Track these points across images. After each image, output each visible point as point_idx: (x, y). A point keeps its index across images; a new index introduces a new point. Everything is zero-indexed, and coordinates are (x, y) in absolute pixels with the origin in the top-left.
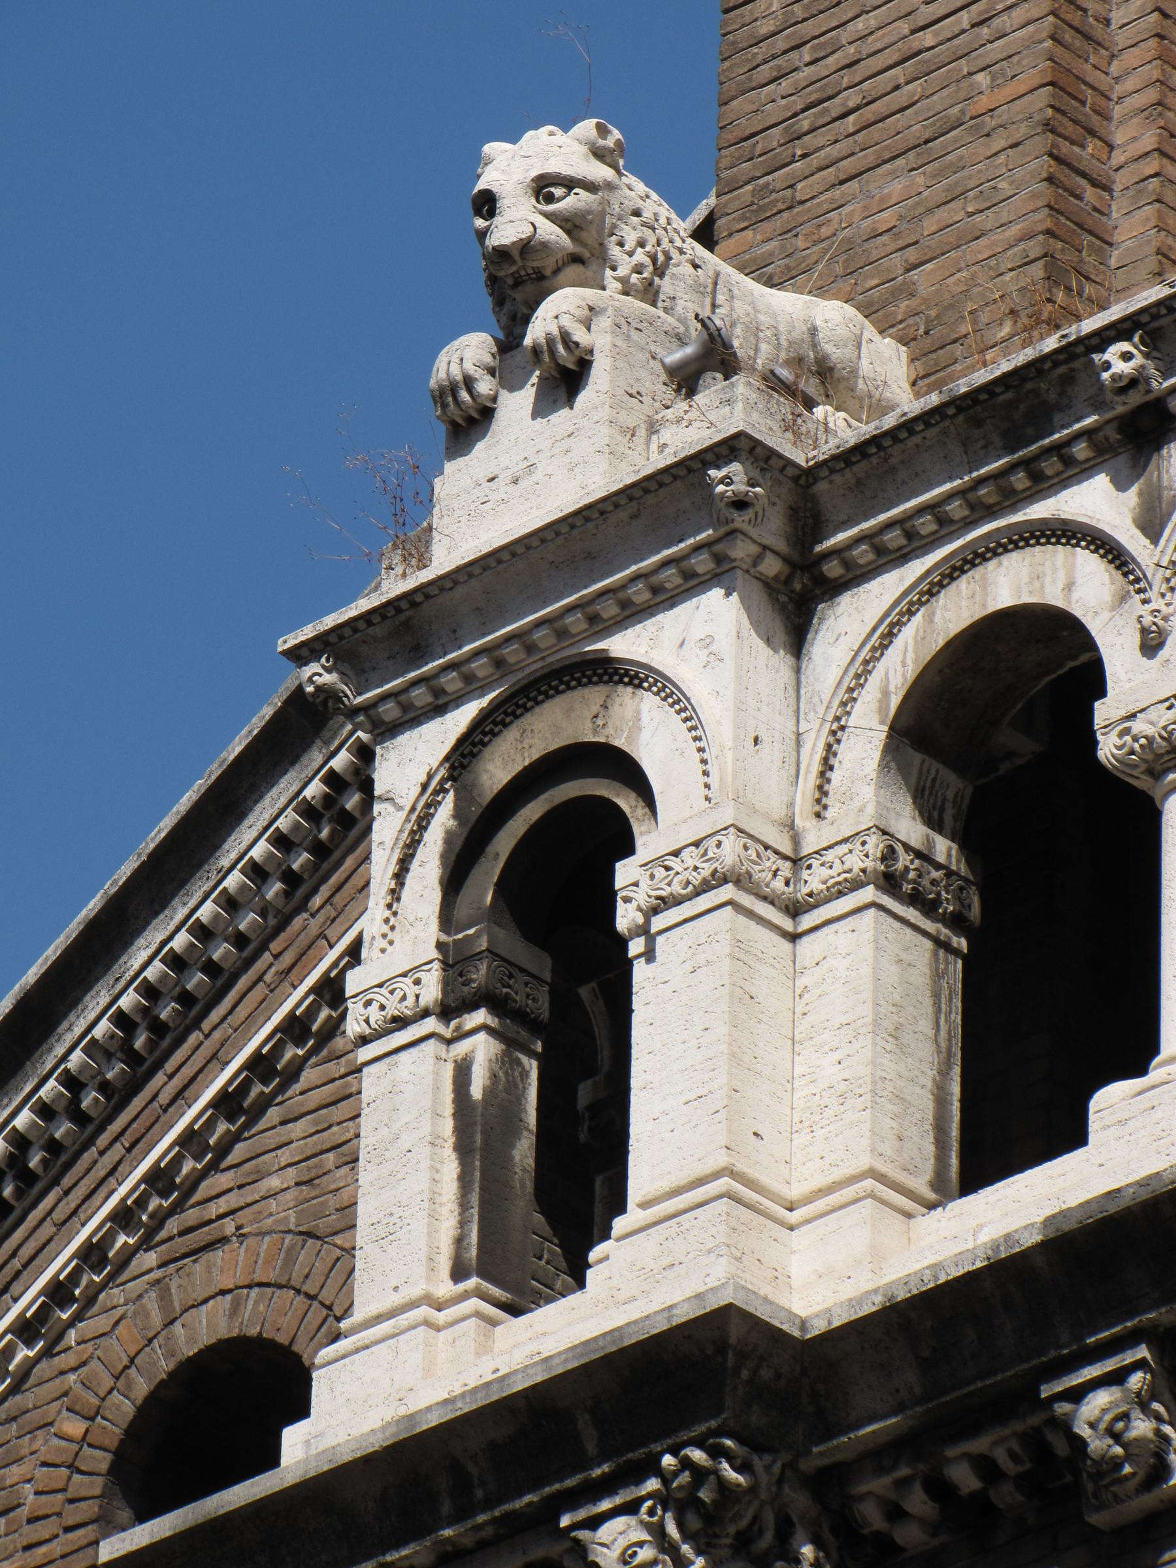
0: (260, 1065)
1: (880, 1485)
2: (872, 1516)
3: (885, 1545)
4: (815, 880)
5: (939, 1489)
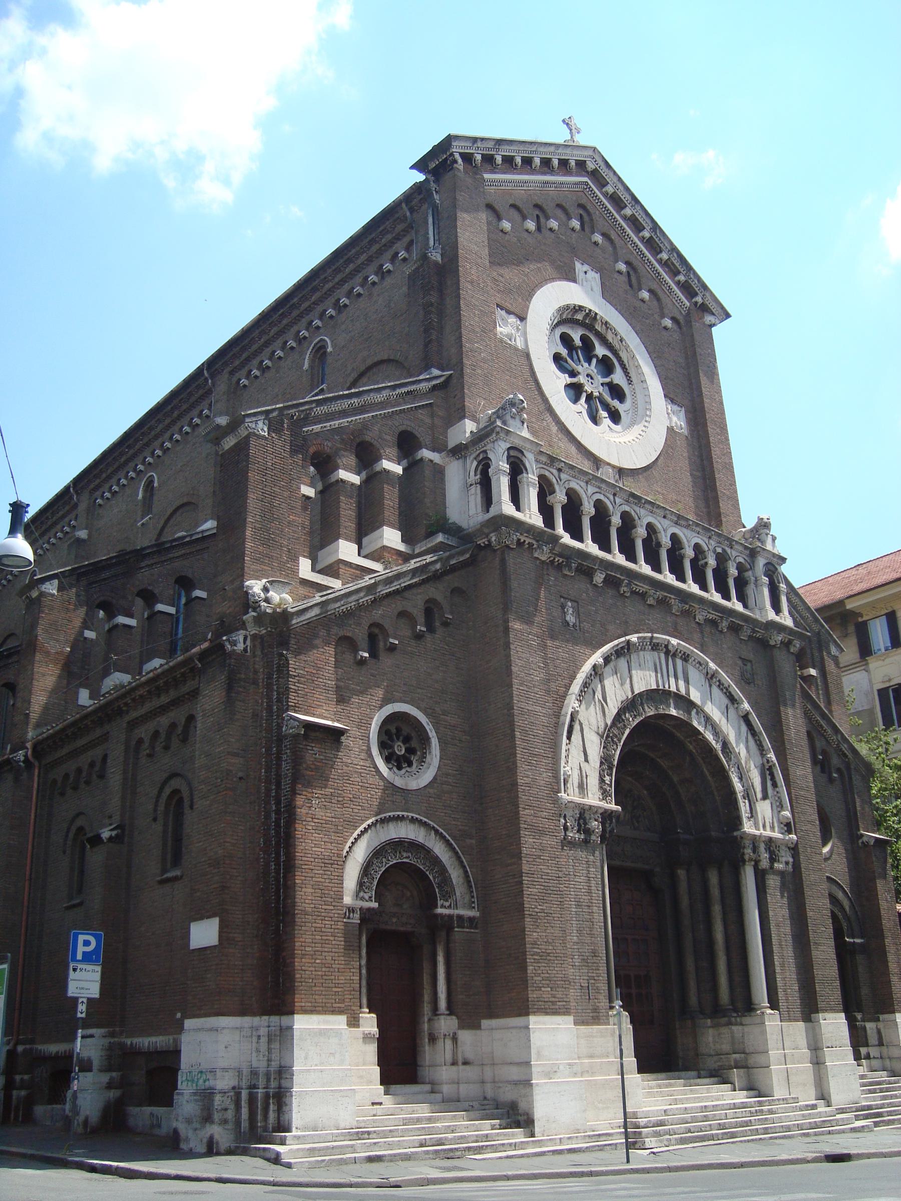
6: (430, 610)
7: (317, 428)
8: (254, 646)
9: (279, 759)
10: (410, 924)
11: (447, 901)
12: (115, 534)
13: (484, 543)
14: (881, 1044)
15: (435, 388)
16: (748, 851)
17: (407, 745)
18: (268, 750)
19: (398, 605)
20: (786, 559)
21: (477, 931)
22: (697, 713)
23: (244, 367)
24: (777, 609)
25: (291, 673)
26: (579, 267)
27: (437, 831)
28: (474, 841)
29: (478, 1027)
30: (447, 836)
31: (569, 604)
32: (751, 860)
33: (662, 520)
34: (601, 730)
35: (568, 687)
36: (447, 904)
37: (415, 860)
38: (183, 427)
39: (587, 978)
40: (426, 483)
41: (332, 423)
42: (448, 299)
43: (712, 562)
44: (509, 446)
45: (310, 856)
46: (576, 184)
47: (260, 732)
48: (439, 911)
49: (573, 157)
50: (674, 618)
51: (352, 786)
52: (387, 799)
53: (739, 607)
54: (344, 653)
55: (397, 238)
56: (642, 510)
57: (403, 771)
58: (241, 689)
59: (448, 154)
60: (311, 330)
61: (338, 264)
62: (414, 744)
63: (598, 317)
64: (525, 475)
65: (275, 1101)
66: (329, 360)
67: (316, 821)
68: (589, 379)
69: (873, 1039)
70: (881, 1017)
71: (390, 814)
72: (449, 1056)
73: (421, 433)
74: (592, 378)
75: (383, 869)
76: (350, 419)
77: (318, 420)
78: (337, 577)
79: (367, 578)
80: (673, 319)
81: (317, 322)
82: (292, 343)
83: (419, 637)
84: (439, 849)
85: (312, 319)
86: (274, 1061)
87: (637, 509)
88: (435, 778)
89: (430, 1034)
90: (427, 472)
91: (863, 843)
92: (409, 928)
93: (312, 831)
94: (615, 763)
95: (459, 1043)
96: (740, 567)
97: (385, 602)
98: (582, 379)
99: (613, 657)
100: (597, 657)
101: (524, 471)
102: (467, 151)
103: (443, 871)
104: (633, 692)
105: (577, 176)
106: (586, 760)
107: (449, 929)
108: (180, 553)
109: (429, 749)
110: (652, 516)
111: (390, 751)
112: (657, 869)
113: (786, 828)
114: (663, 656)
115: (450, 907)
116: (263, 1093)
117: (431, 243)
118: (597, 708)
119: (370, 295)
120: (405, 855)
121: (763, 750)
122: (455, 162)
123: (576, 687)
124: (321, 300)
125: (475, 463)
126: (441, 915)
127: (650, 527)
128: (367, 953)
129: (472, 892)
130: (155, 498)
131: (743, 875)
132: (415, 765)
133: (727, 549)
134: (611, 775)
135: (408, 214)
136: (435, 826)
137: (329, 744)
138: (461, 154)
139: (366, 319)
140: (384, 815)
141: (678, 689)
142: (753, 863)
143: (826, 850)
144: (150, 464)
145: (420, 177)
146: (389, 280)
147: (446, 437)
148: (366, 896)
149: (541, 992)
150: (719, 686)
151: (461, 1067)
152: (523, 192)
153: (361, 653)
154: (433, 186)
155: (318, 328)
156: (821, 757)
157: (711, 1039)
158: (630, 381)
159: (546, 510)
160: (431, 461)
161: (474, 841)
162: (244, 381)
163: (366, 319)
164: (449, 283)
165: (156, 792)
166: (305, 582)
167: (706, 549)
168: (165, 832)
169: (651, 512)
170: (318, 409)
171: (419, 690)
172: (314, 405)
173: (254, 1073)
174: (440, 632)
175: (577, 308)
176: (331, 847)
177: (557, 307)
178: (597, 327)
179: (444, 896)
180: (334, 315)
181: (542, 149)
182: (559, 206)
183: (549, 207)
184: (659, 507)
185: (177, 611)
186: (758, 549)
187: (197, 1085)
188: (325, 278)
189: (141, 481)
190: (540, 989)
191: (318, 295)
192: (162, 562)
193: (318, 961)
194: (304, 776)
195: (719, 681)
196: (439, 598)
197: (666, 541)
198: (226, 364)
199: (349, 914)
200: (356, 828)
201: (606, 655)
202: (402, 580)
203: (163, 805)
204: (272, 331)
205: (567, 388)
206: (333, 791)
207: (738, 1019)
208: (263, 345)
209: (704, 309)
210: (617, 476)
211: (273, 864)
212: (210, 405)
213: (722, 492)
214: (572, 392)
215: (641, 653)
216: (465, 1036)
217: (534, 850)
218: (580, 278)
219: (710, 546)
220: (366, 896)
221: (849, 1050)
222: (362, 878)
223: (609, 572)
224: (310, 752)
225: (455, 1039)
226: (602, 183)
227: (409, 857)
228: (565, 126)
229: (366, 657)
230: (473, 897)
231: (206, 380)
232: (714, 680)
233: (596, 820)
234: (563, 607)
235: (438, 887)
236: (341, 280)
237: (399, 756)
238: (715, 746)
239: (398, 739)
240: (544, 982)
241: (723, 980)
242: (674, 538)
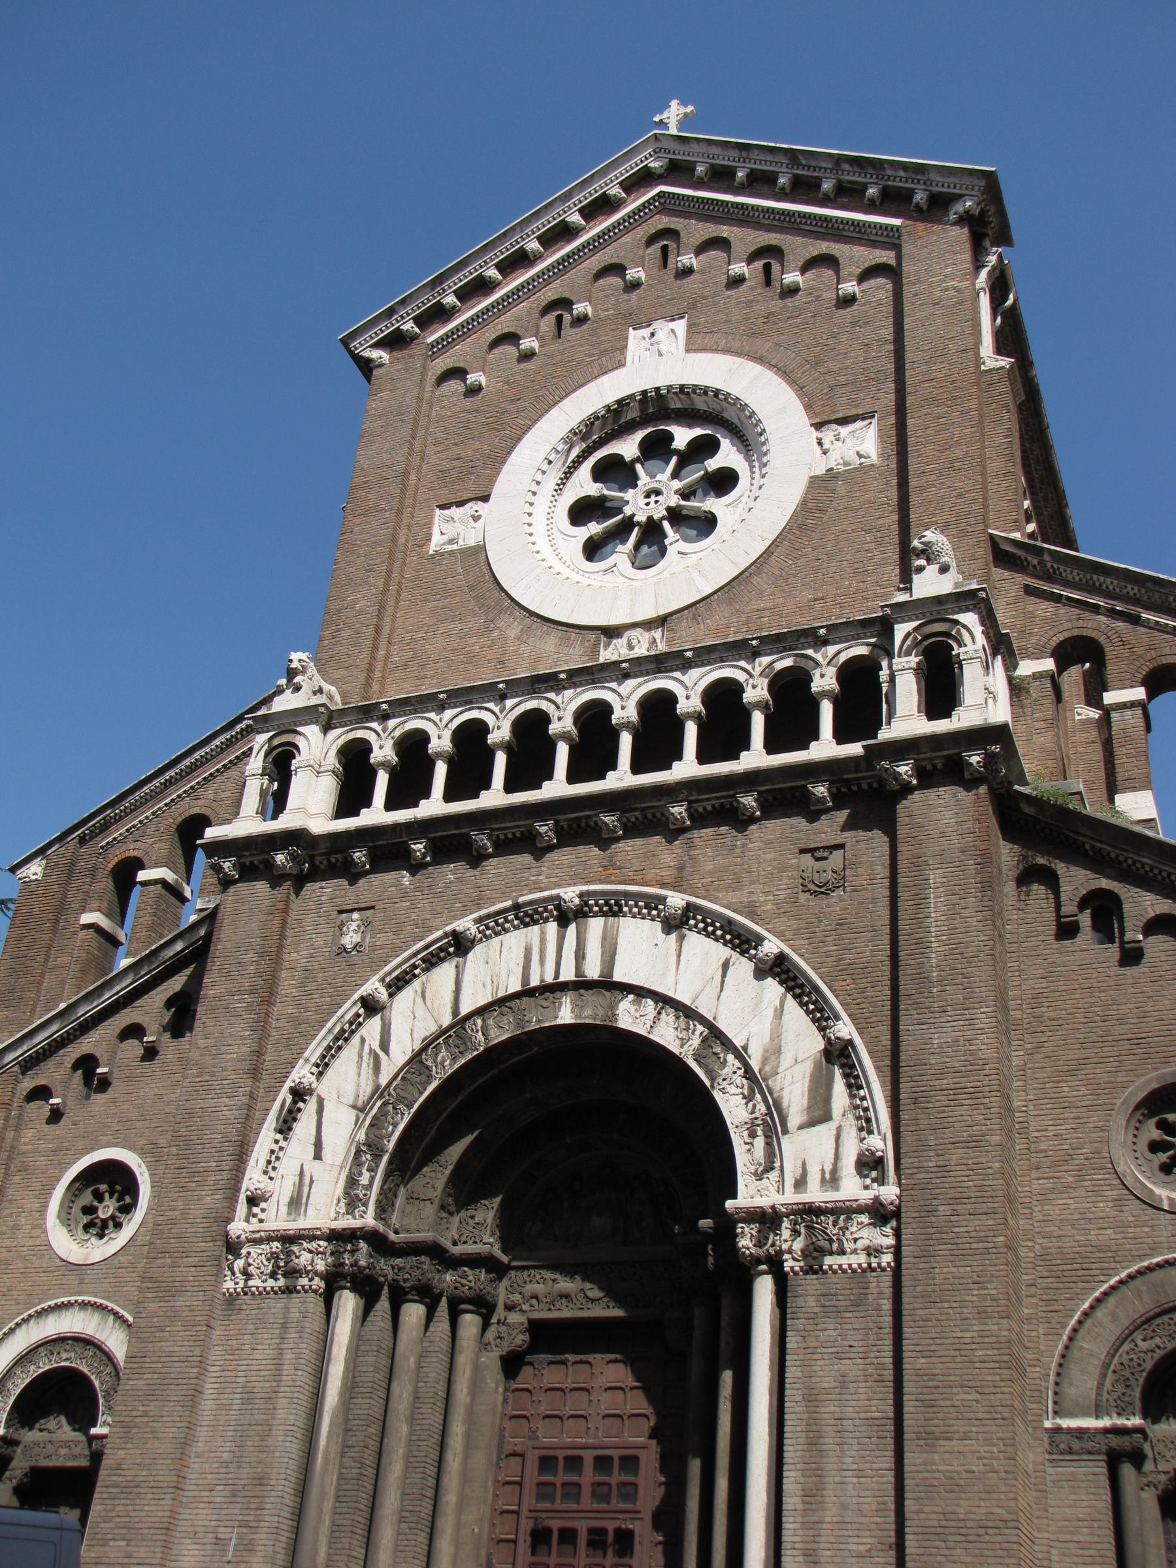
0: (211, 775)
1: (319, 858)
2: (317, 862)
3: (318, 867)
4: (322, 769)
5: (329, 861)
94: (391, 1145)
106: (318, 1156)
118: (364, 1065)
120: (64, 1355)
178: (673, 406)
202: (118, 988)
223: (432, 835)
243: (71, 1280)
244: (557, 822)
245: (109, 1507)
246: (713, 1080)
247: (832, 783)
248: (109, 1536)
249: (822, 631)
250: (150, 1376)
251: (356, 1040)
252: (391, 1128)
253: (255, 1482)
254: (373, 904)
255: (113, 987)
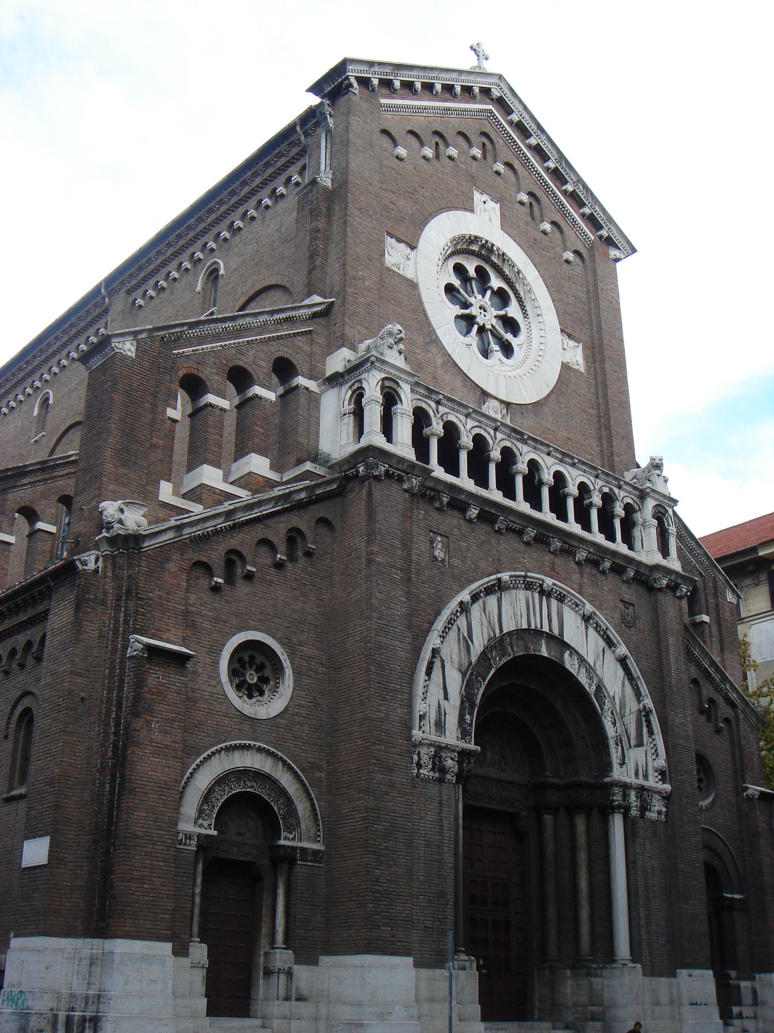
6: (294, 537)
7: (188, 350)
8: (106, 567)
9: (122, 681)
10: (252, 854)
11: (291, 833)
12: (10, 450)
13: (352, 473)
14: (755, 1003)
15: (315, 315)
16: (618, 798)
17: (260, 674)
18: (112, 670)
19: (259, 532)
20: (678, 501)
21: (321, 865)
22: (571, 655)
23: (140, 287)
24: (665, 553)
25: (140, 596)
26: (478, 197)
27: (285, 763)
28: (323, 775)
29: (315, 963)
30: (295, 767)
31: (439, 538)
32: (619, 807)
33: (546, 457)
34: (464, 668)
35: (431, 623)
36: (291, 836)
37: (260, 790)
38: (79, 345)
39: (432, 919)
40: (299, 411)
41: (204, 347)
42: (335, 225)
43: (597, 500)
44: (384, 375)
45: (145, 779)
46: (480, 111)
47: (106, 653)
48: (282, 842)
49: (477, 86)
50: (552, 557)
51: (198, 712)
52: (234, 727)
53: (623, 549)
54: (198, 578)
55: (291, 162)
56: (523, 446)
57: (254, 700)
58: (89, 610)
59: (343, 77)
60: (207, 251)
61: (233, 187)
62: (268, 673)
63: (495, 248)
64: (399, 406)
65: (92, 1025)
66: (221, 282)
67: (155, 744)
68: (482, 311)
69: (747, 997)
70: (757, 976)
71: (236, 742)
72: (282, 991)
73: (298, 360)
74: (485, 311)
75: (225, 797)
76: (223, 344)
77: (189, 343)
78: (200, 502)
79: (226, 504)
80: (577, 253)
81: (212, 244)
82: (187, 264)
83: (279, 566)
84: (286, 780)
85: (207, 241)
86: (95, 984)
87: (519, 445)
88: (286, 708)
89: (265, 967)
90: (303, 400)
91: (747, 795)
92: (250, 858)
93: (148, 755)
94: (478, 701)
95: (294, 979)
96: (628, 508)
97: (245, 529)
98: (474, 310)
99: (482, 595)
100: (465, 596)
101: (399, 402)
102: (363, 75)
103: (289, 802)
104: (501, 630)
105: (480, 103)
106: (446, 697)
107: (292, 862)
108: (64, 472)
109: (283, 679)
110: (535, 453)
111: (242, 679)
112: (524, 813)
113: (660, 777)
114: (536, 595)
115: (294, 839)
116: (80, 1016)
117: (323, 167)
118: (462, 646)
119: (263, 219)
120: (249, 784)
121: (641, 696)
122: (351, 85)
123: (439, 624)
124: (216, 222)
125: (350, 393)
126: (284, 846)
127: (532, 464)
128: (203, 881)
129: (319, 825)
130: (50, 415)
131: (612, 824)
132: (267, 693)
133: (614, 488)
134: (471, 714)
135: (302, 138)
136: (283, 756)
137: (173, 669)
138: (357, 78)
139: (257, 243)
140: (230, 743)
141: (550, 629)
142: (622, 811)
143: (704, 803)
144: (46, 381)
145: (315, 100)
146: (282, 205)
147: (325, 365)
148: (206, 824)
149: (380, 931)
150: (596, 628)
151: (294, 1003)
152: (422, 118)
153: (215, 579)
154: (328, 110)
155: (212, 250)
156: (707, 706)
157: (569, 990)
158: (525, 315)
159: (420, 442)
160: (307, 389)
161: (323, 775)
162: (139, 301)
163: (257, 243)
164: (337, 208)
165: (9, 709)
166: (165, 505)
167: (592, 487)
168: (15, 750)
169: (535, 449)
170: (190, 331)
171: (277, 620)
172: (185, 328)
173: (72, 996)
174: (302, 561)
175: (472, 238)
176: (168, 772)
177: (451, 236)
178: (493, 259)
179: (288, 828)
180: (228, 237)
181: (443, 75)
182: (461, 134)
183: (449, 134)
184: (542, 444)
185: (59, 530)
186: (648, 490)
187: (16, 1005)
188: (221, 200)
189: (37, 398)
190: (379, 927)
191: (213, 217)
192: (45, 479)
193: (146, 886)
194: (144, 699)
195: (597, 623)
196: (303, 528)
197: (548, 477)
198: (122, 283)
199: (186, 841)
200: (199, 756)
201: (474, 593)
202: (263, 508)
203: (15, 723)
204: (169, 251)
205: (459, 320)
206: (174, 715)
207: (598, 971)
208: (159, 266)
209: (609, 242)
210: (505, 411)
211: (108, 785)
212: (107, 324)
213: (616, 431)
214: (463, 324)
215: (514, 591)
216: (302, 973)
217: (382, 786)
218: (479, 208)
219: (598, 487)
220: (206, 824)
221: (714, 1012)
222: (202, 804)
224: (153, 675)
225: (289, 974)
226: (507, 109)
227: (253, 787)
228: (473, 51)
229: (220, 583)
230: (319, 830)
231: (104, 298)
232: (592, 621)
233: (452, 759)
234: (432, 541)
235: (282, 819)
236: (236, 203)
237: (250, 685)
238: (588, 690)
239: (251, 668)
240: (384, 921)
241: (585, 930)
242: (558, 476)
243: (246, 727)
244: (562, 546)
245: (377, 906)
246: (602, 711)
247: (133, 360)
248: (381, 924)
249: (526, 437)
250: (385, 824)
251: (455, 627)
252: (476, 691)
253: (440, 896)
254: (448, 535)
255: (261, 506)
